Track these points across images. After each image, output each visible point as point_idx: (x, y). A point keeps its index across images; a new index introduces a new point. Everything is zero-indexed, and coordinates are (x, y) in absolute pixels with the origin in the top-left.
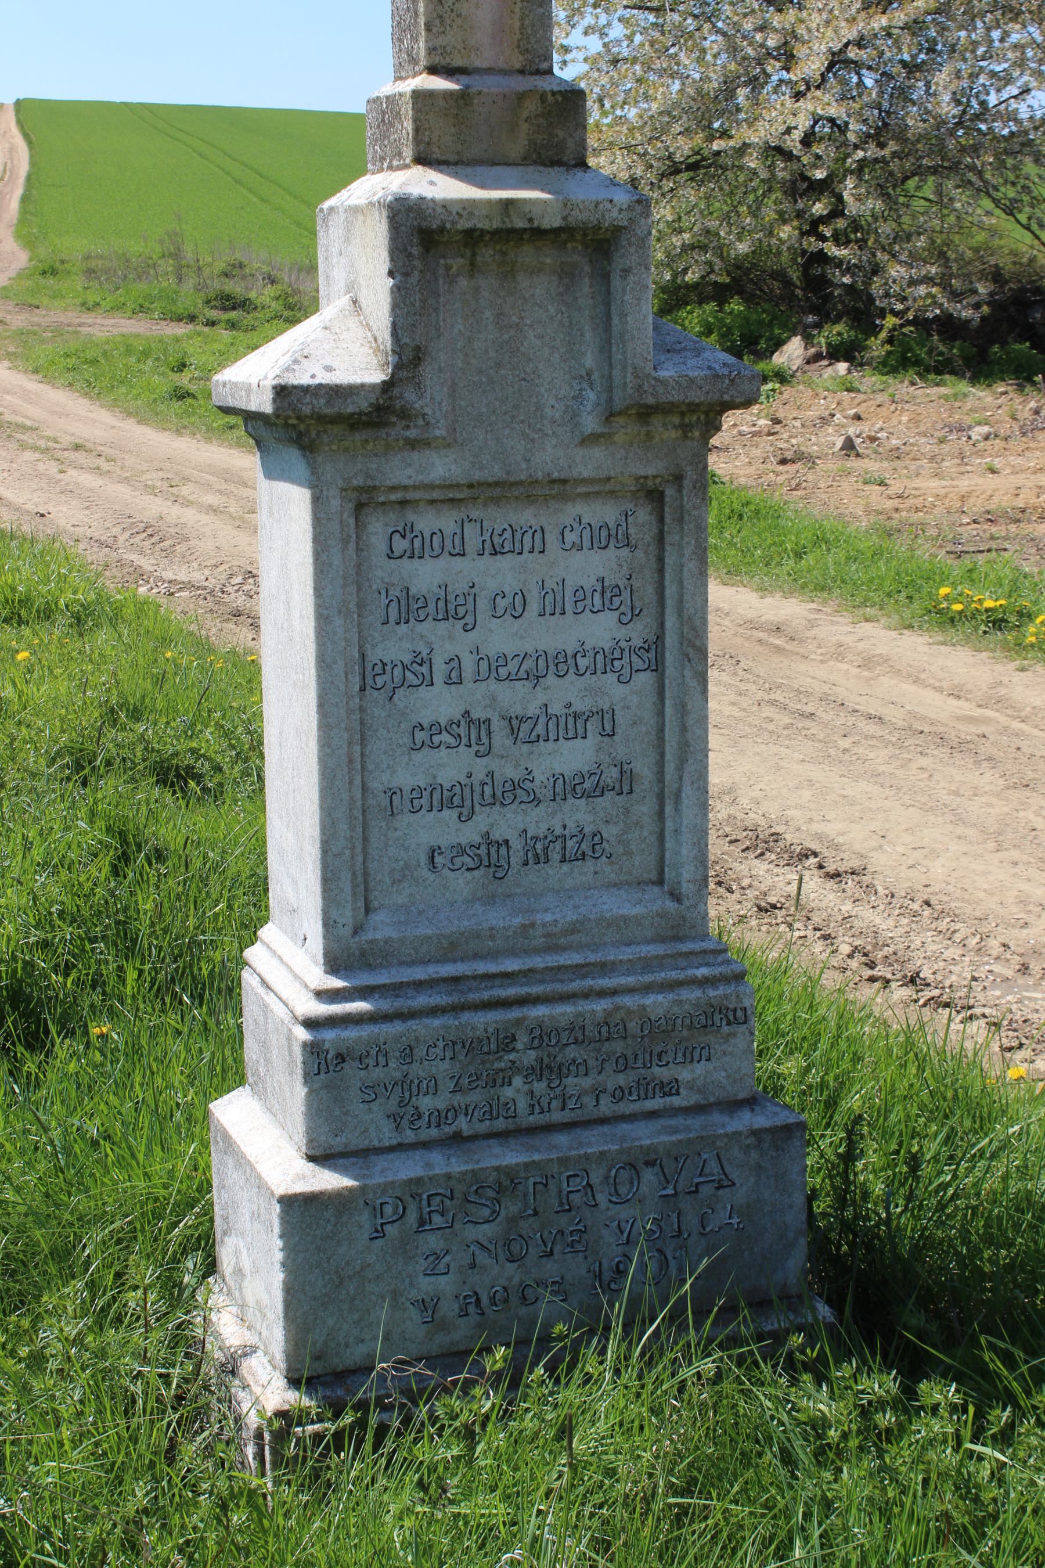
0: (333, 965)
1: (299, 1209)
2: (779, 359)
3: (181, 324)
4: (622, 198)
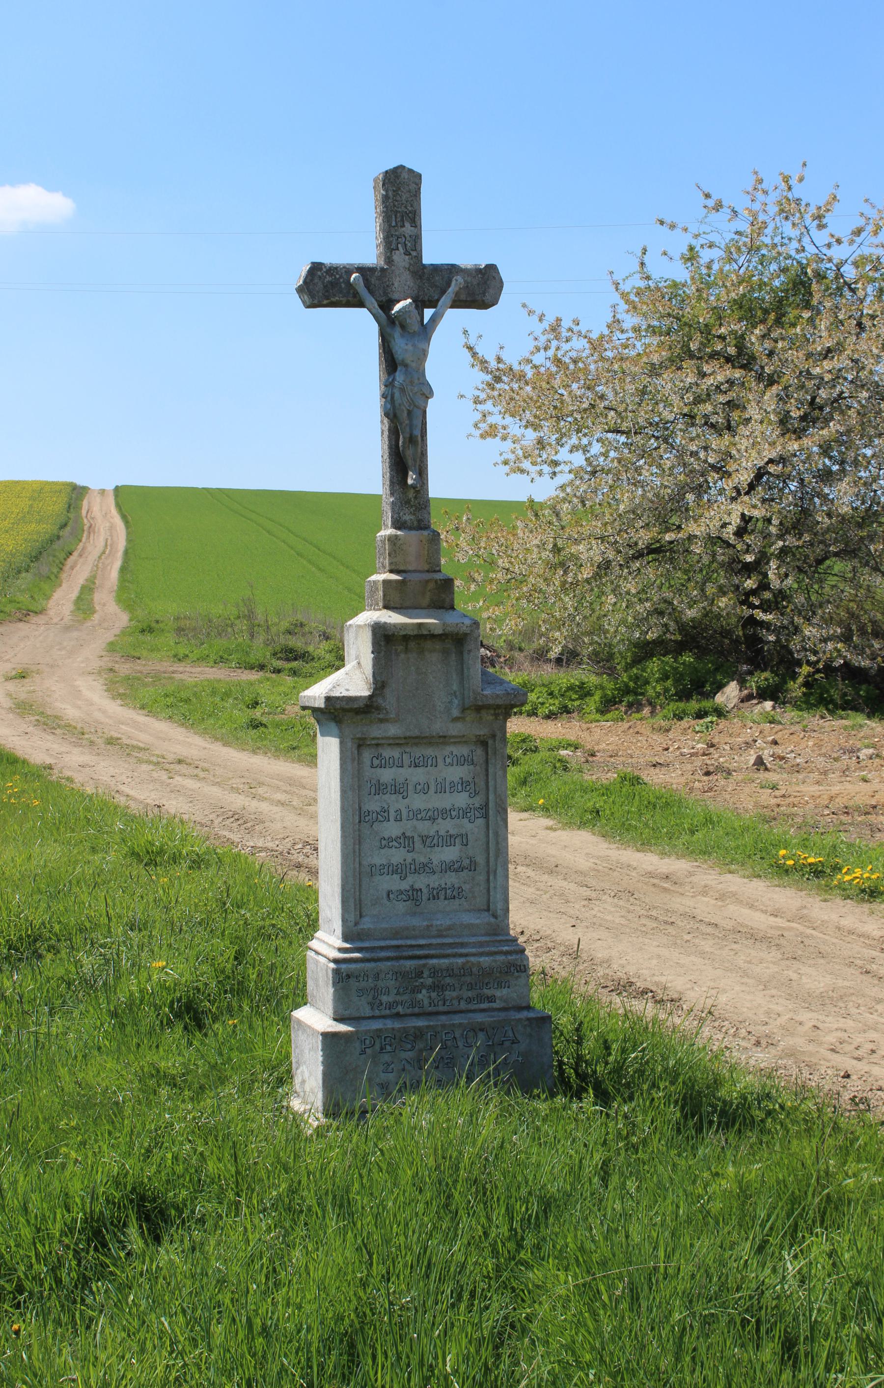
0: (346, 938)
1: (329, 1038)
2: (719, 698)
3: (253, 671)
4: (467, 622)
